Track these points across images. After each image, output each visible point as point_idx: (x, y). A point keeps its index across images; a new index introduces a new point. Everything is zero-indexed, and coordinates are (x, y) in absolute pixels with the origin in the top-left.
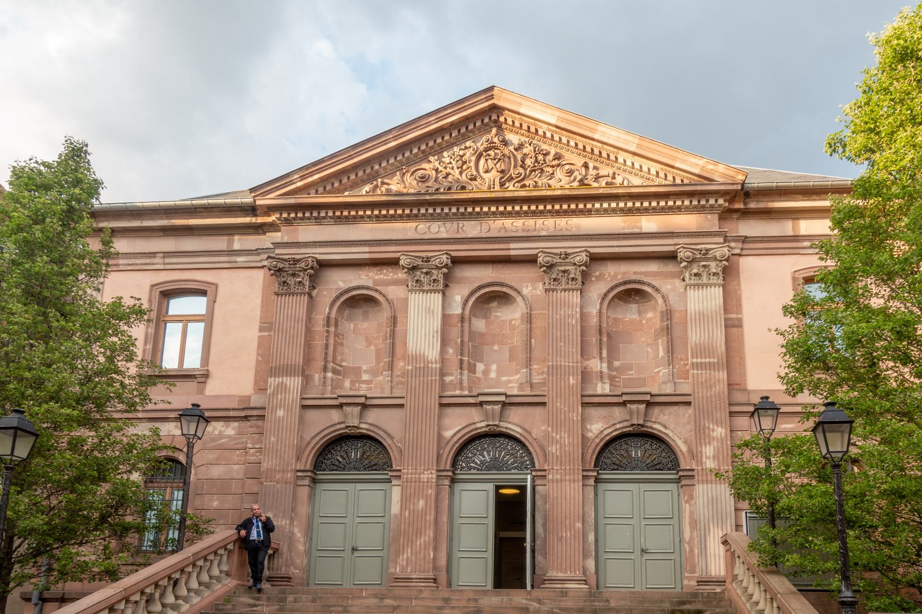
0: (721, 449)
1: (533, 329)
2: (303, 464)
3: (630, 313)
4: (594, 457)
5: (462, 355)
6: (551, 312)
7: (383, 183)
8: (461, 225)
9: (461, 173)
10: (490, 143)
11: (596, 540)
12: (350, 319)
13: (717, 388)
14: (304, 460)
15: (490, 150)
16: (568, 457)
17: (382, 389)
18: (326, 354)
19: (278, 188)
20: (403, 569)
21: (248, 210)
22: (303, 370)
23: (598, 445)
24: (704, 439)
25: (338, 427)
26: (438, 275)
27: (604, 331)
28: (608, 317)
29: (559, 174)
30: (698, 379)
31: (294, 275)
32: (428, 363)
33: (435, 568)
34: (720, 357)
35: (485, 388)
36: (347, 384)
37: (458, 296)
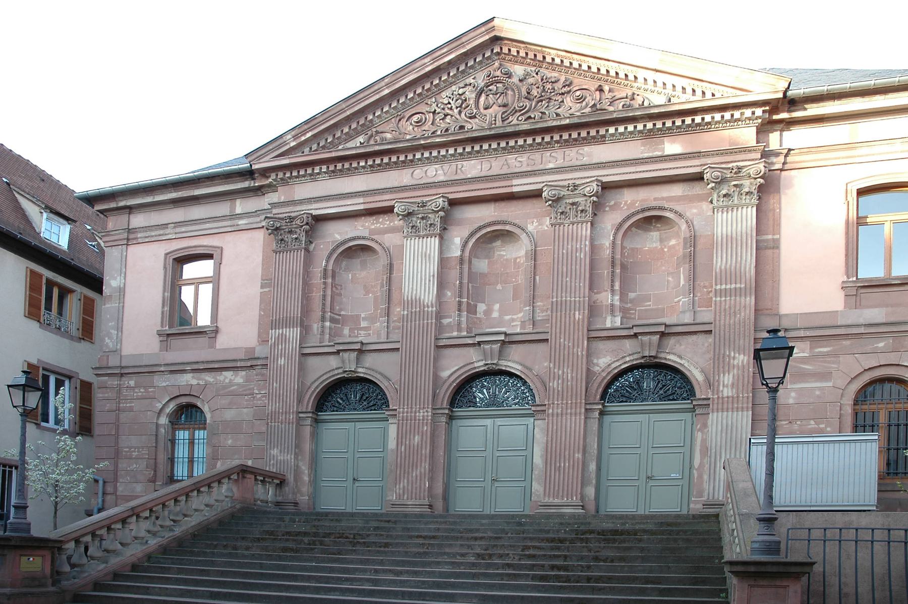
0: (741, 377)
1: (537, 266)
3: (651, 240)
4: (600, 390)
5: (460, 296)
6: (556, 248)
7: (377, 132)
8: (460, 167)
9: (460, 112)
10: (492, 78)
11: (599, 469)
12: (347, 269)
13: (743, 314)
14: (305, 403)
15: (492, 84)
16: (570, 391)
17: (379, 335)
18: (324, 304)
19: (272, 150)
20: (399, 497)
21: (246, 175)
22: (302, 321)
23: (604, 378)
24: (723, 367)
25: (336, 372)
26: (436, 219)
27: (618, 262)
28: (623, 248)
29: (568, 101)
30: (720, 306)
31: (290, 232)
32: (424, 307)
33: (431, 495)
34: (748, 282)
35: (486, 328)
36: (346, 331)
37: (456, 240)
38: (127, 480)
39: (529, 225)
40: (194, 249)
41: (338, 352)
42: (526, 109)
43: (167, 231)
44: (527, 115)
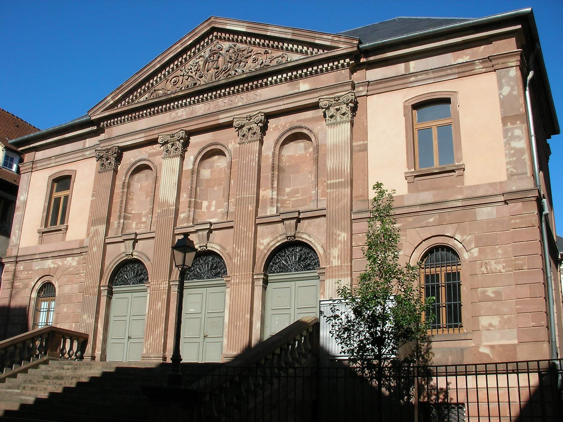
2: (104, 282)
6: (240, 159)
10: (212, 52)
23: (266, 254)
35: (208, 219)
36: (134, 225)
39: (229, 145)
41: (283, 221)
42: (228, 69)
43: (52, 161)
44: (228, 73)
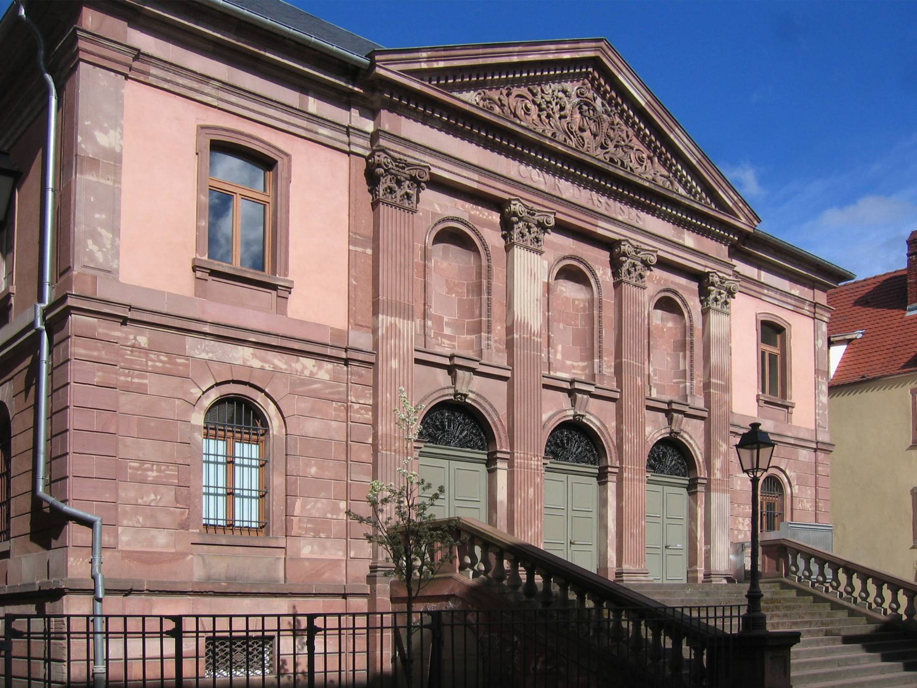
38: (138, 522)
40: (248, 139)
43: (207, 89)
